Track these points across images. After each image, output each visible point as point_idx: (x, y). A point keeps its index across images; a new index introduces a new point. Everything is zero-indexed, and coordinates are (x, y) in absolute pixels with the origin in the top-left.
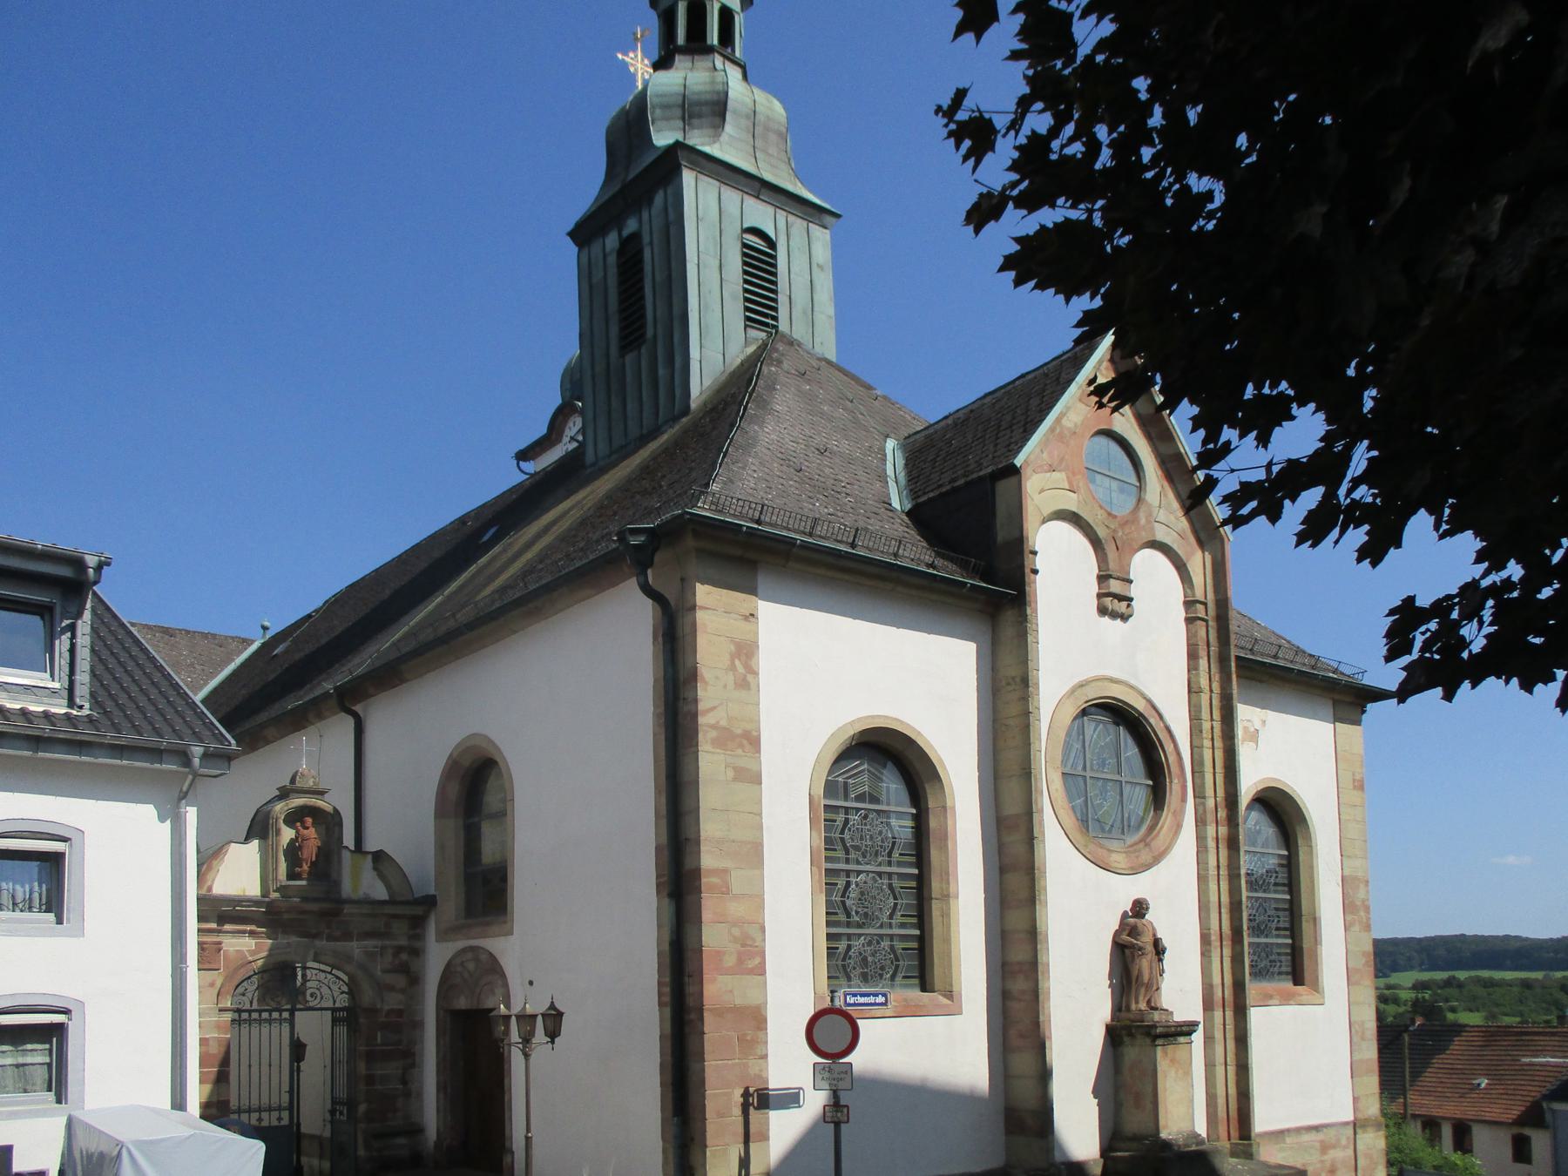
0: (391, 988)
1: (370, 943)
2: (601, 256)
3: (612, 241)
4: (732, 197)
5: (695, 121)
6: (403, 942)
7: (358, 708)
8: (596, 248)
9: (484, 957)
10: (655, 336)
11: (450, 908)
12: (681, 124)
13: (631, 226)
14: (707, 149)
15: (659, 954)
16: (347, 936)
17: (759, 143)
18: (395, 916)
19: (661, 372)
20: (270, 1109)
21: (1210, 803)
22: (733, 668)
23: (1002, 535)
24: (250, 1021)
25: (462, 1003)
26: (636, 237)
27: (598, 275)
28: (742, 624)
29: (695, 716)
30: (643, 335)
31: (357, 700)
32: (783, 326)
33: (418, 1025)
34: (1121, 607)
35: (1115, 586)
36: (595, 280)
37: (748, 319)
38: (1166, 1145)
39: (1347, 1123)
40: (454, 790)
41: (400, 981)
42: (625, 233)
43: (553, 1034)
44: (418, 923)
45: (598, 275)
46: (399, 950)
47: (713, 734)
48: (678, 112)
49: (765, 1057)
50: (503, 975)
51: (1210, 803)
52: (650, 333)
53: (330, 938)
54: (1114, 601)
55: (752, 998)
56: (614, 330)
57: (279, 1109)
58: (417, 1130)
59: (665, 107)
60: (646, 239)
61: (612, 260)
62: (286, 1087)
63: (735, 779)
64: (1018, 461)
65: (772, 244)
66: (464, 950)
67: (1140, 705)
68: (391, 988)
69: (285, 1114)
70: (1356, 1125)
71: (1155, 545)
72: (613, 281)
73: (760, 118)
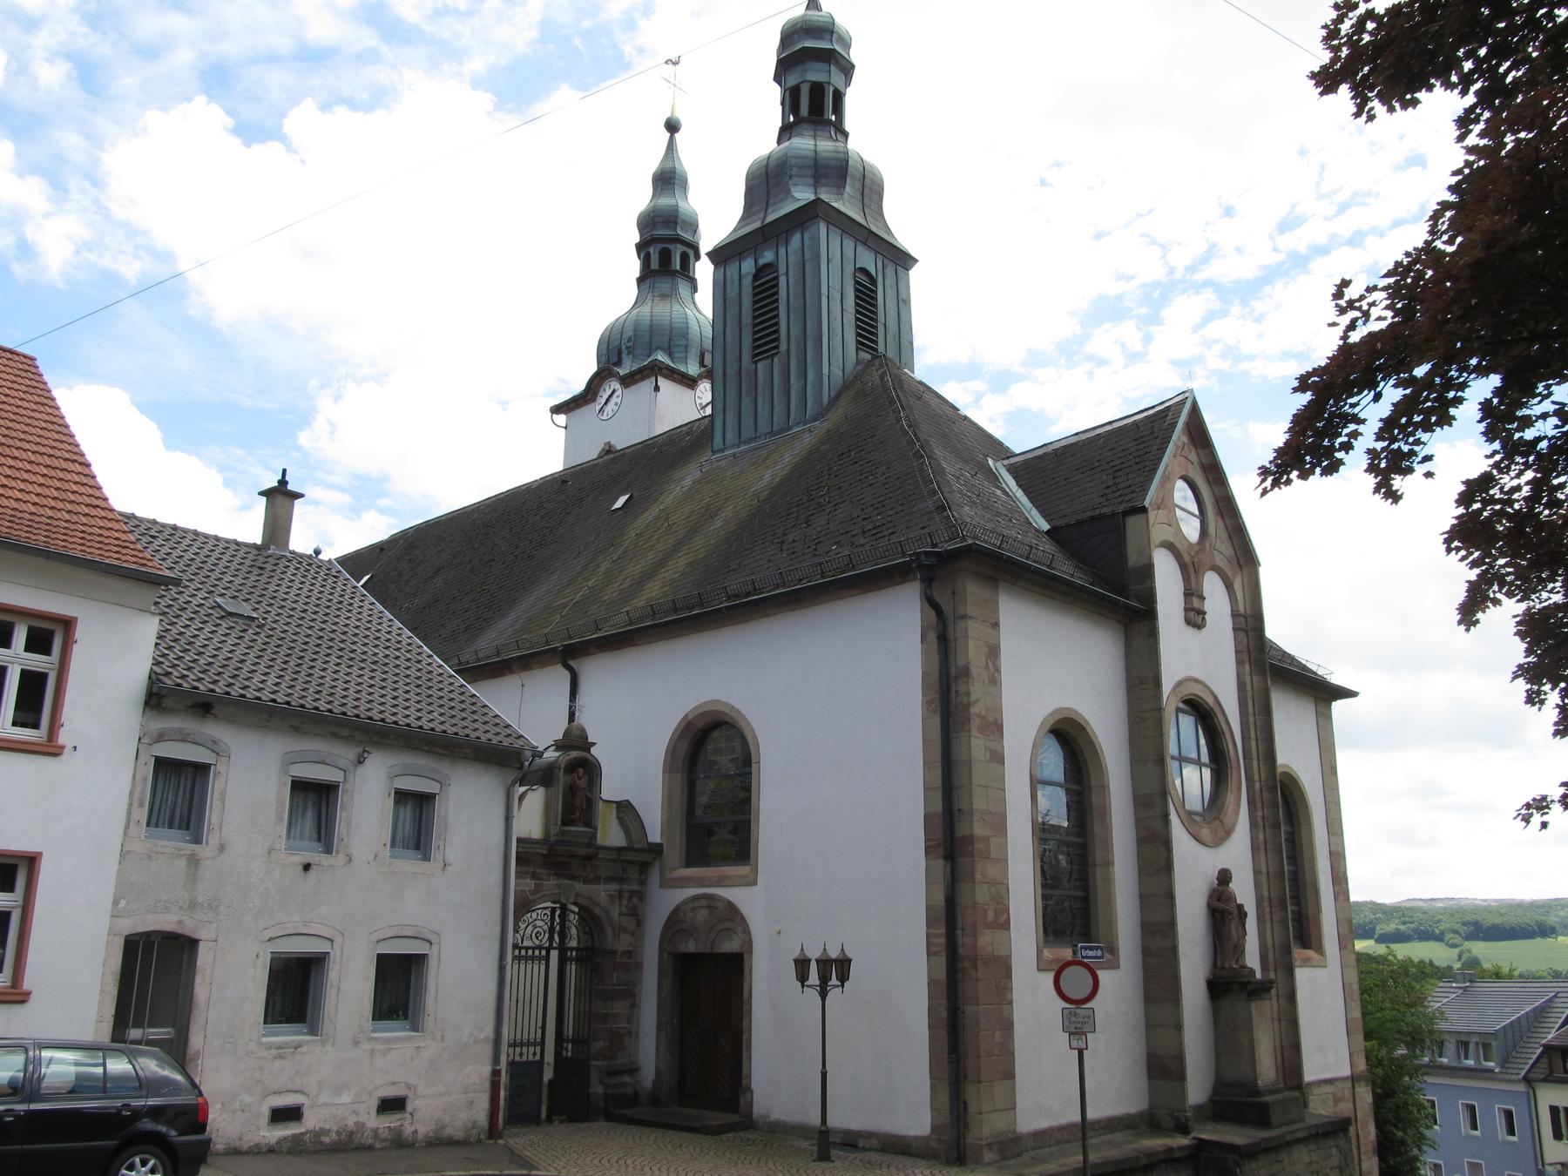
0: (625, 930)
1: (615, 886)
2: (736, 277)
3: (748, 266)
4: (849, 245)
5: (823, 181)
6: (635, 887)
7: (571, 663)
8: (732, 270)
9: (720, 905)
10: (788, 350)
11: (674, 853)
12: (811, 181)
13: (768, 257)
14: (835, 205)
15: (928, 909)
16: (597, 880)
17: (866, 201)
18: (632, 862)
19: (793, 380)
20: (528, 1044)
21: (1257, 786)
22: (987, 667)
23: (1133, 559)
24: (526, 958)
25: (691, 947)
26: (771, 267)
27: (733, 291)
28: (990, 630)
29: (967, 706)
30: (777, 347)
31: (574, 657)
32: (881, 348)
33: (638, 966)
34: (1199, 619)
35: (1196, 603)
36: (729, 296)
37: (859, 342)
38: (1211, 1101)
39: (1346, 1078)
40: (684, 748)
41: (629, 923)
42: (761, 262)
43: (843, 978)
44: (645, 867)
45: (733, 291)
46: (632, 893)
47: (978, 722)
48: (810, 172)
49: (1011, 1003)
50: (743, 920)
51: (1257, 786)
52: (783, 347)
53: (587, 881)
54: (1195, 617)
55: (729, 946)
56: (747, 341)
57: (535, 1044)
58: (634, 1070)
59: (801, 167)
60: (782, 269)
61: (747, 281)
62: (540, 1024)
63: (991, 760)
64: (1147, 503)
65: (873, 281)
66: (696, 898)
67: (1210, 701)
68: (625, 930)
69: (538, 1049)
70: (1354, 1079)
71: (1215, 568)
72: (747, 300)
73: (867, 181)
